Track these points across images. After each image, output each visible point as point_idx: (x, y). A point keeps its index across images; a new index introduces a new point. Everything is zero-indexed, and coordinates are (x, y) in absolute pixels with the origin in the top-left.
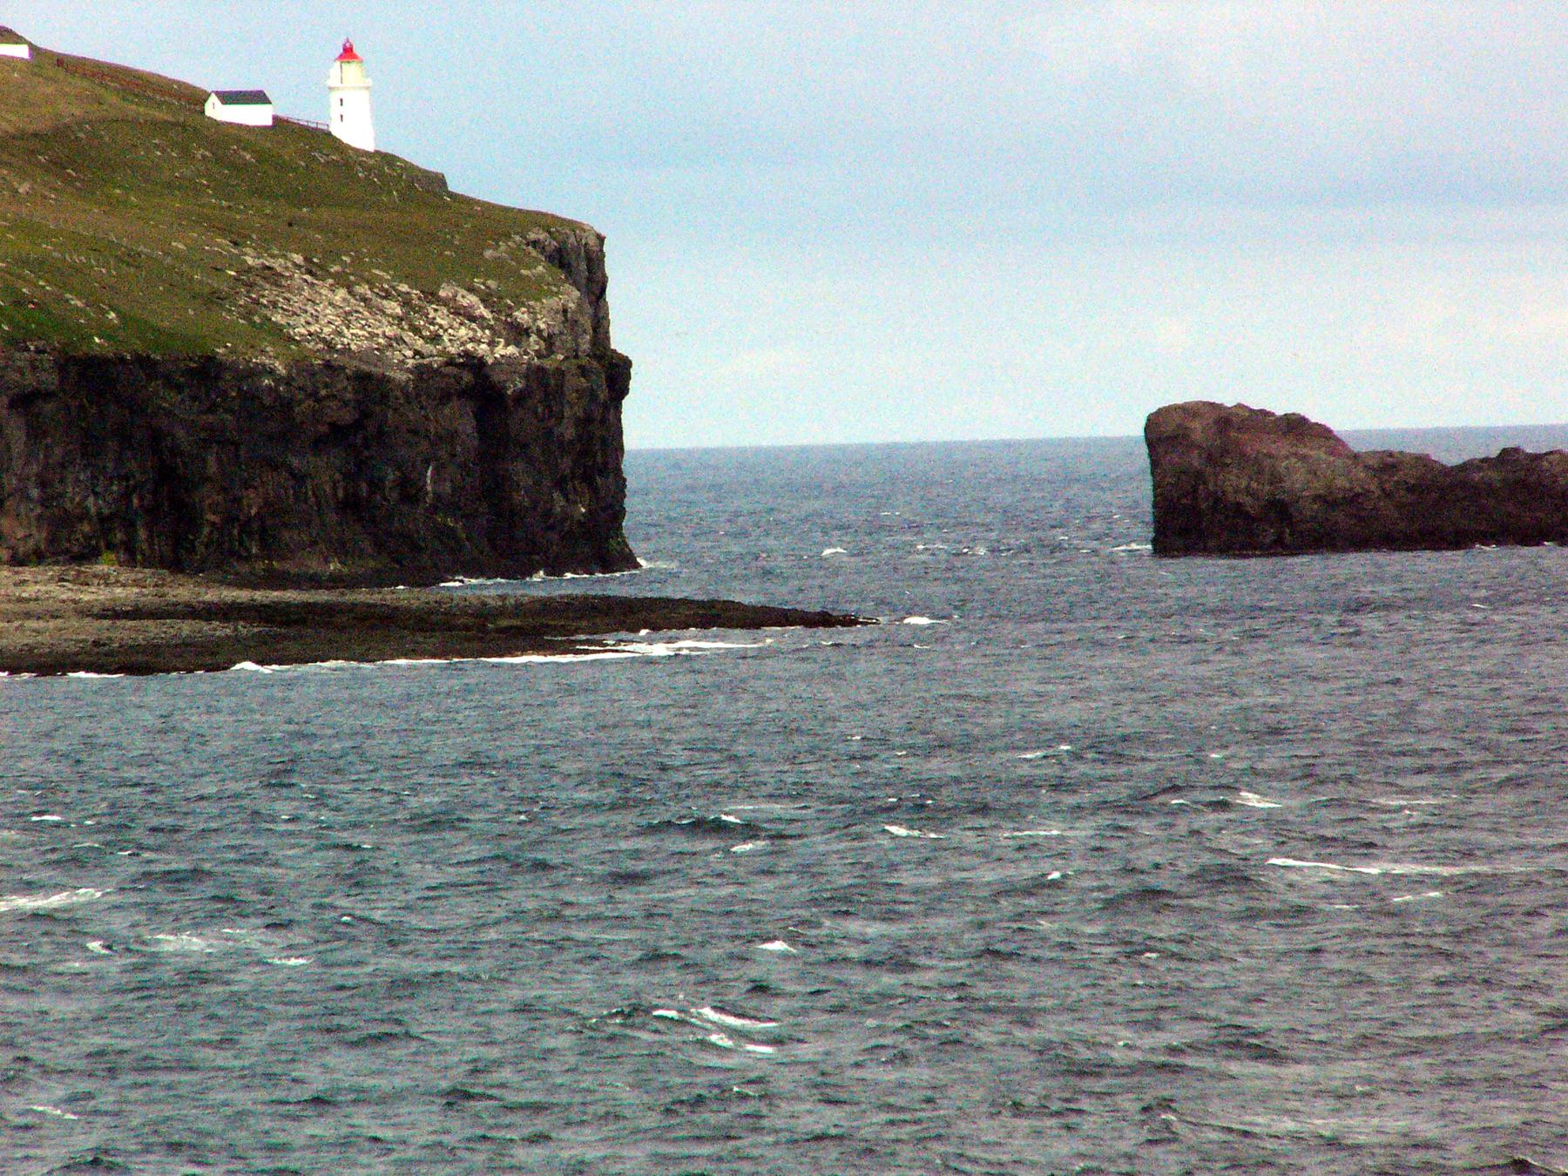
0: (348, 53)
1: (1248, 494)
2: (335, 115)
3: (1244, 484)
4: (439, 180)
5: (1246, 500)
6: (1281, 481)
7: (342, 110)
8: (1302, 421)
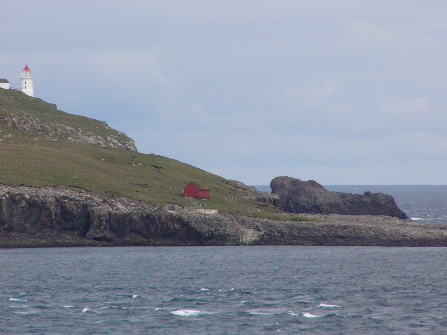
0: (26, 69)
1: (307, 203)
2: (23, 87)
3: (306, 200)
4: (54, 106)
5: (307, 205)
6: (317, 199)
7: (26, 85)
8: (315, 182)
